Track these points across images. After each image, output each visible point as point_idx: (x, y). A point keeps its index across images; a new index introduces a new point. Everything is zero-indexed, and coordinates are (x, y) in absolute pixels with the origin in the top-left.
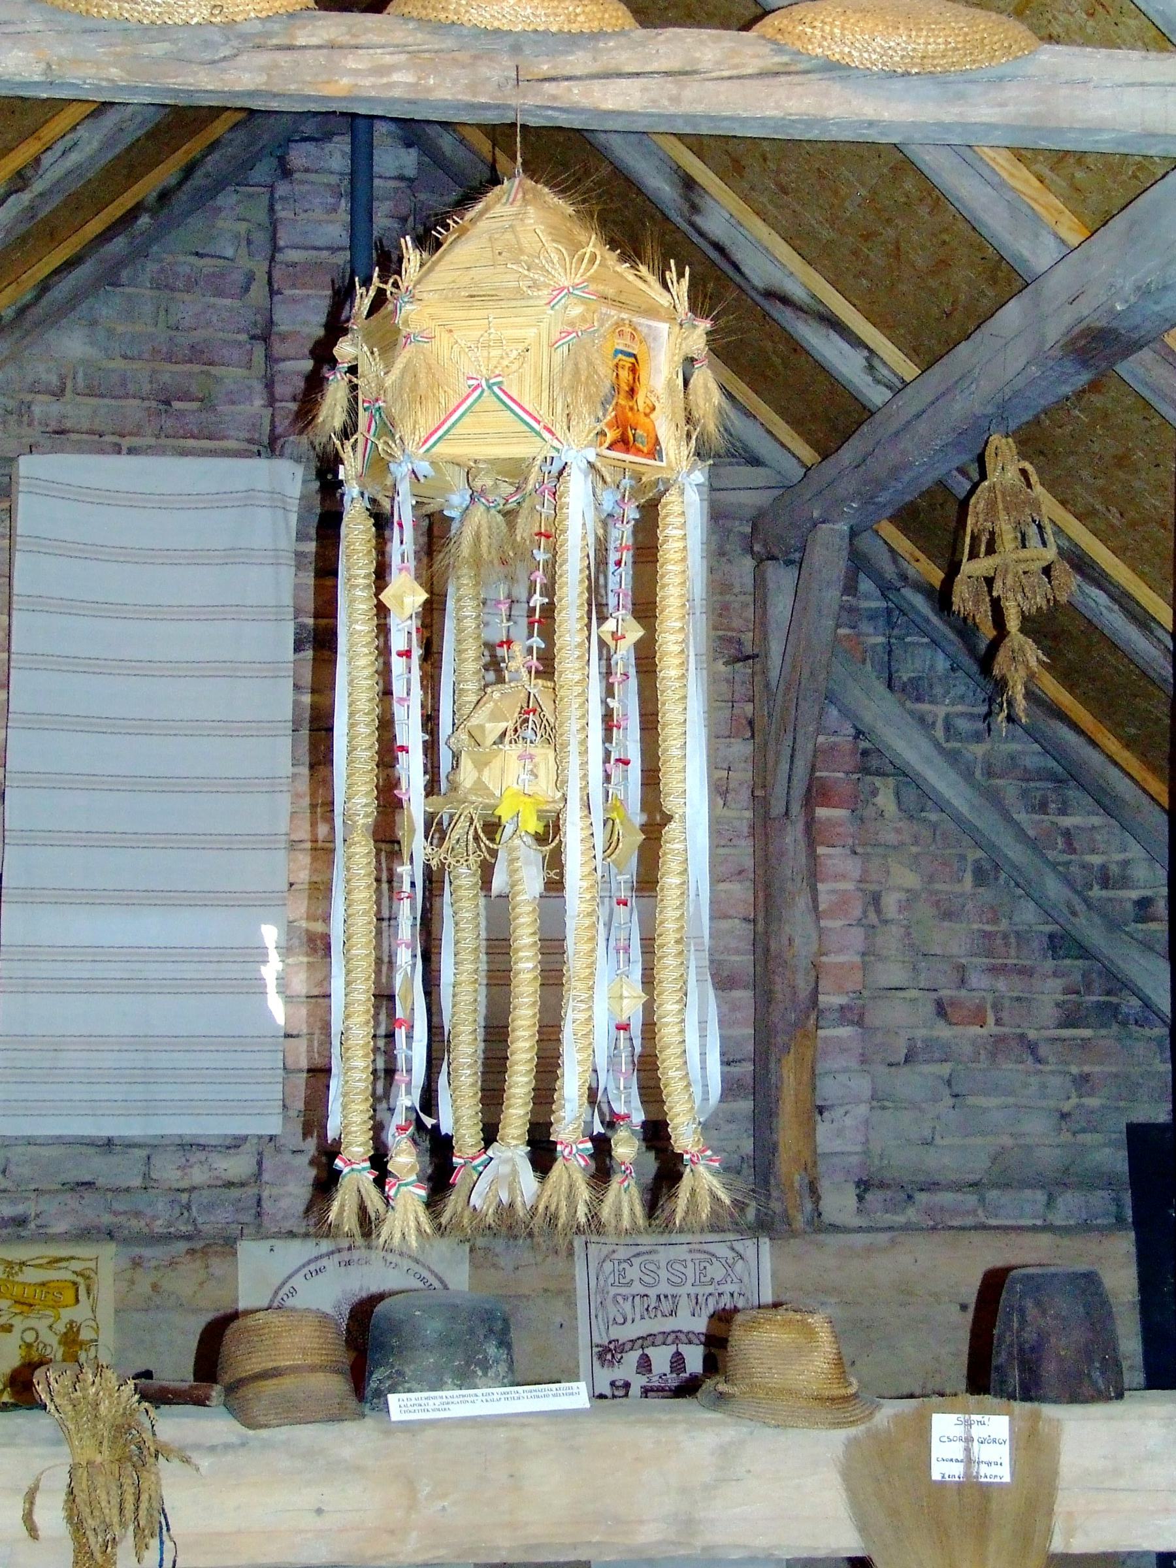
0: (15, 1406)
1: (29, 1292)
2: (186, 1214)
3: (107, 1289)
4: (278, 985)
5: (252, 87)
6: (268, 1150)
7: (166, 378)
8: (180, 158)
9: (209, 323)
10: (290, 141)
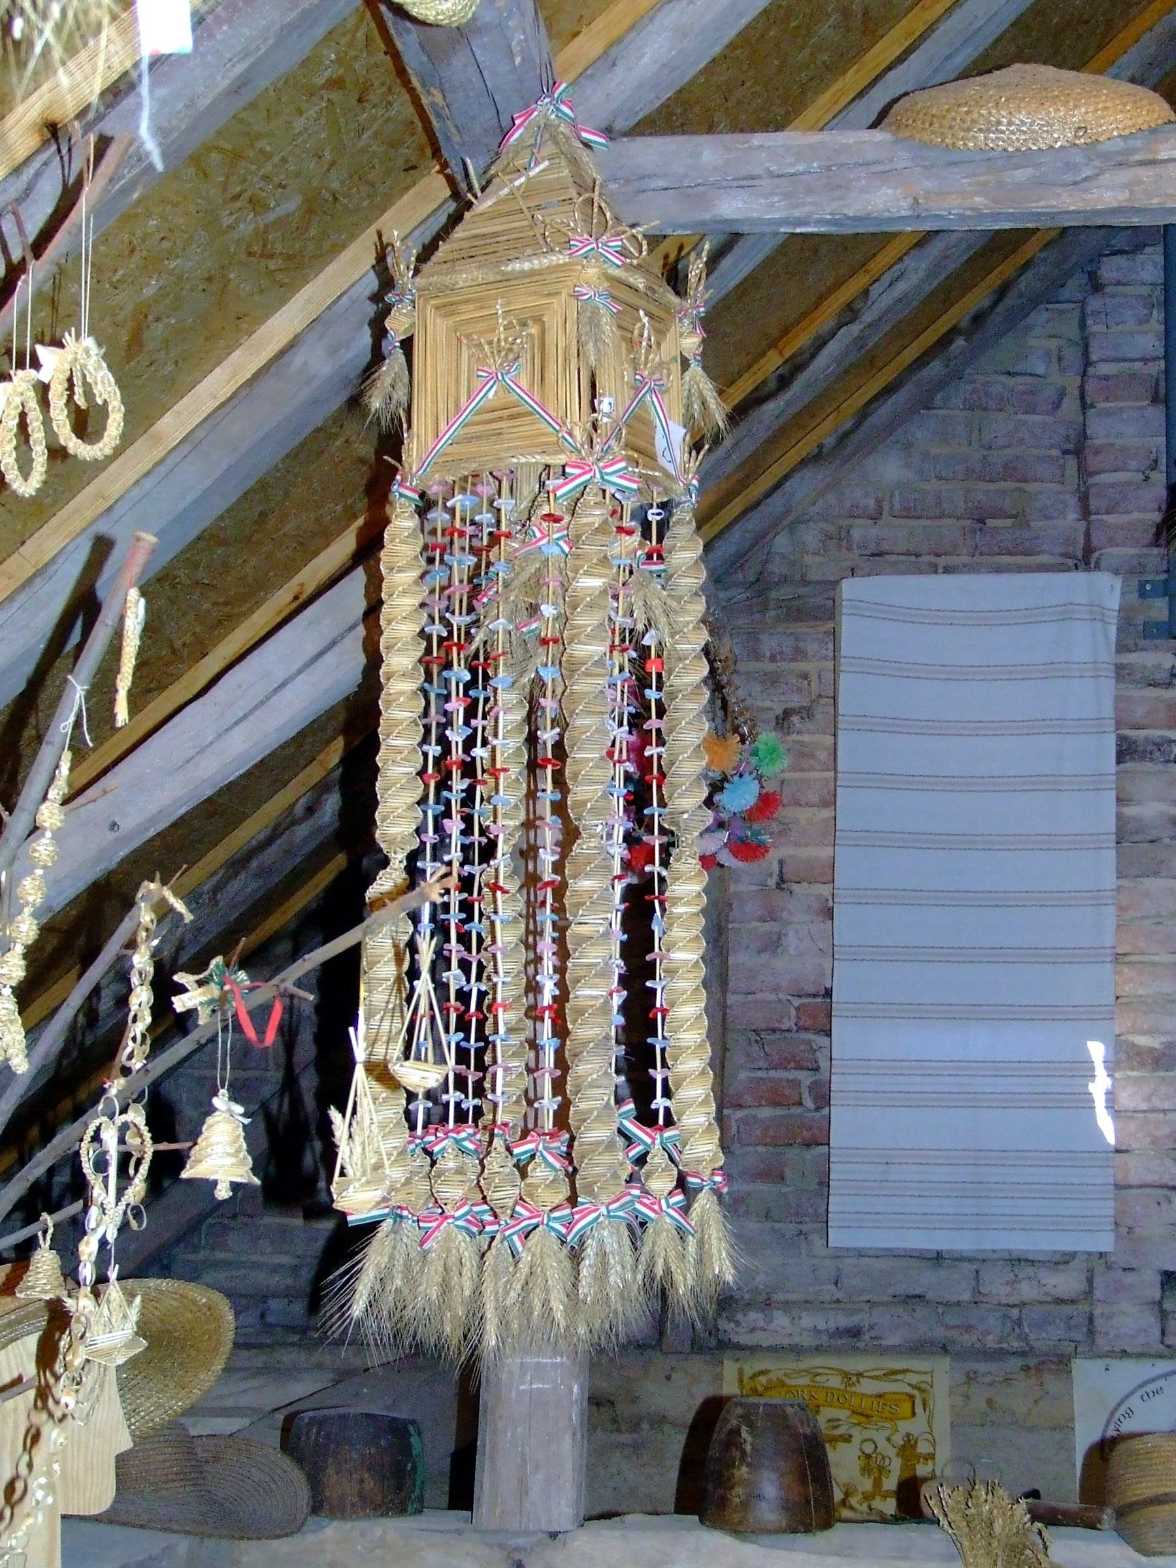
0: (896, 1520)
1: (866, 1404)
2: (1017, 1330)
3: (942, 1404)
4: (1107, 1100)
5: (1114, 204)
6: (1099, 1267)
7: (980, 496)
8: (994, 280)
9: (1022, 441)
10: (1101, 255)
